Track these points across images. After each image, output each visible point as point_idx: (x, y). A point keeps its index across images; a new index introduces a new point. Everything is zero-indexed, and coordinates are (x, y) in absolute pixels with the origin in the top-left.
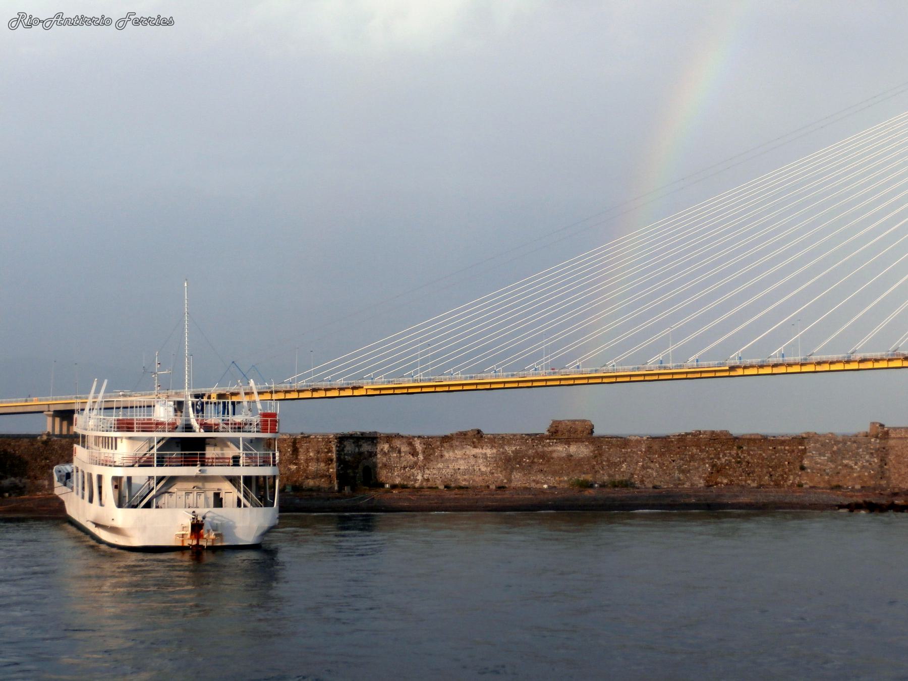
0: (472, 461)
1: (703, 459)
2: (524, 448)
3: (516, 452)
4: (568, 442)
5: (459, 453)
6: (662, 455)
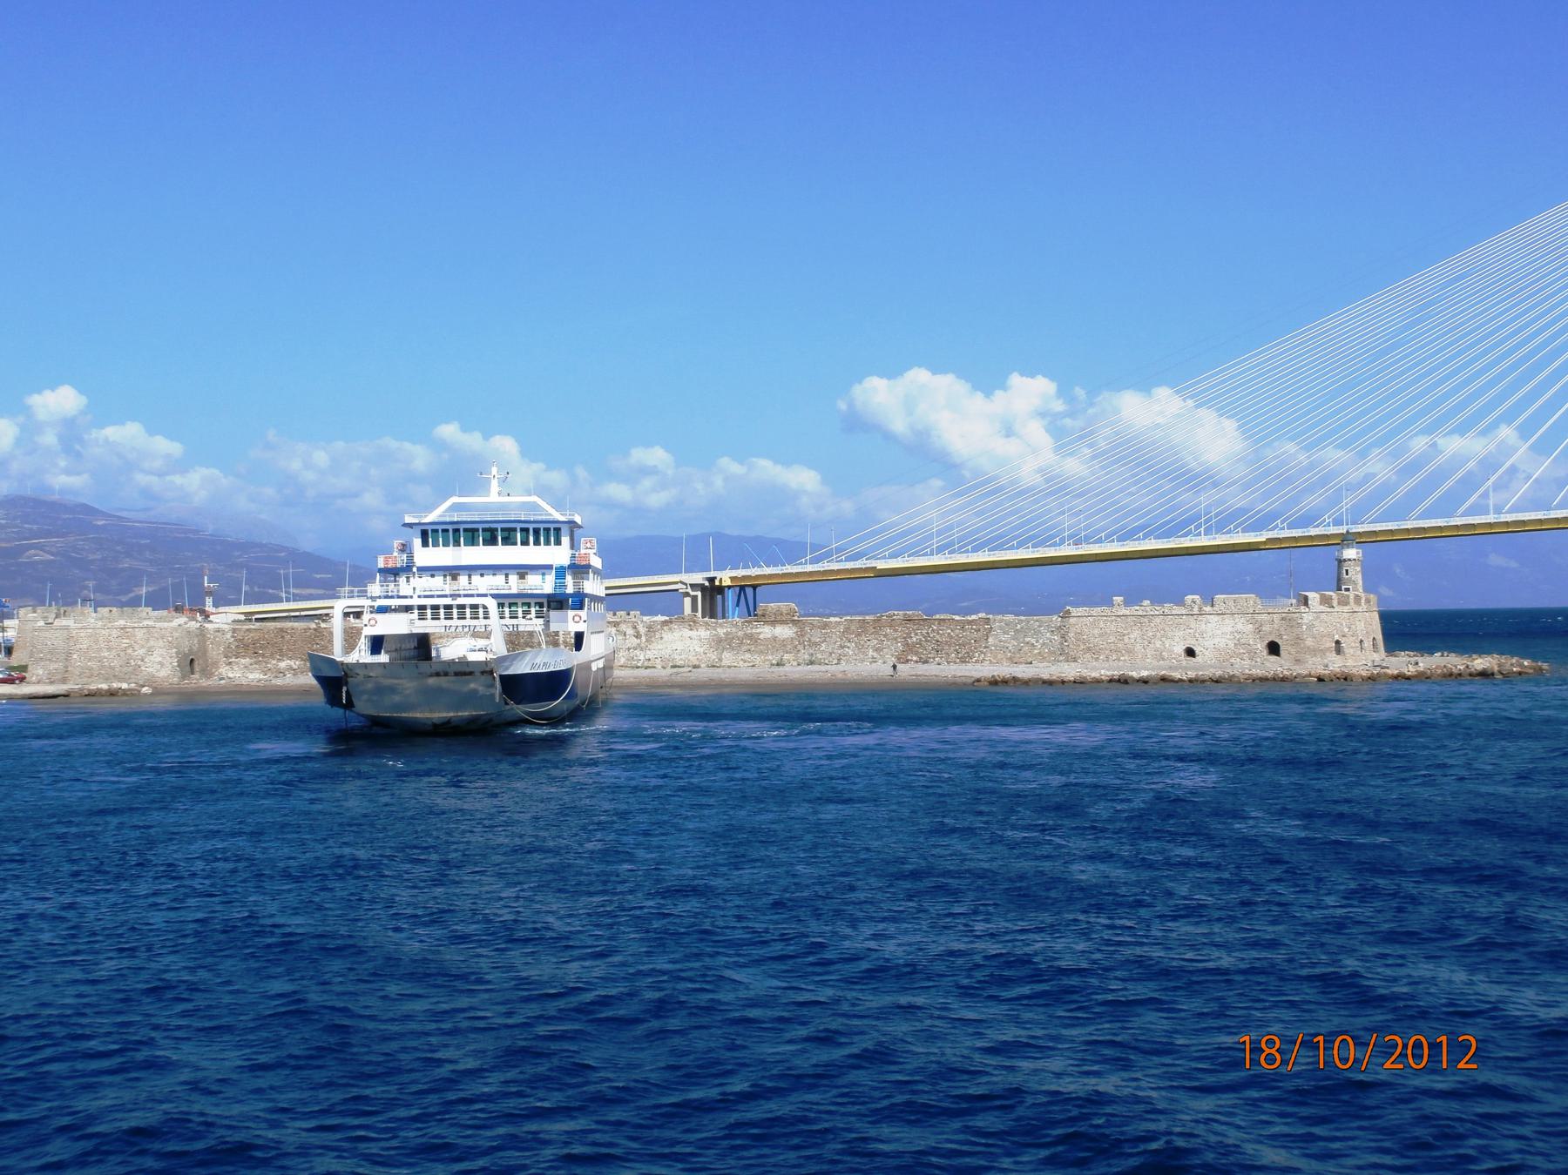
0: (688, 642)
1: (896, 639)
2: (734, 630)
3: (727, 634)
4: (773, 623)
5: (677, 634)
6: (859, 635)
